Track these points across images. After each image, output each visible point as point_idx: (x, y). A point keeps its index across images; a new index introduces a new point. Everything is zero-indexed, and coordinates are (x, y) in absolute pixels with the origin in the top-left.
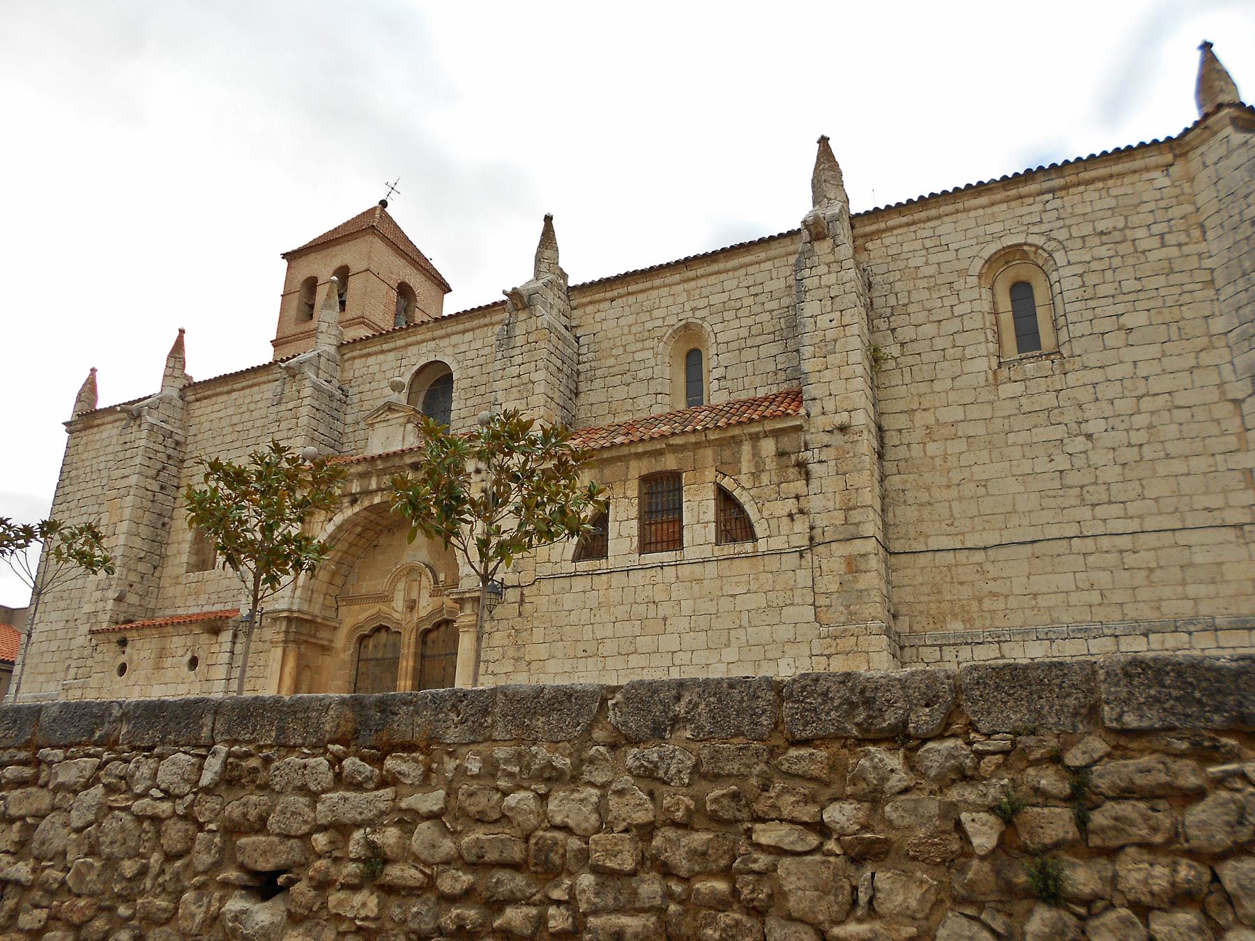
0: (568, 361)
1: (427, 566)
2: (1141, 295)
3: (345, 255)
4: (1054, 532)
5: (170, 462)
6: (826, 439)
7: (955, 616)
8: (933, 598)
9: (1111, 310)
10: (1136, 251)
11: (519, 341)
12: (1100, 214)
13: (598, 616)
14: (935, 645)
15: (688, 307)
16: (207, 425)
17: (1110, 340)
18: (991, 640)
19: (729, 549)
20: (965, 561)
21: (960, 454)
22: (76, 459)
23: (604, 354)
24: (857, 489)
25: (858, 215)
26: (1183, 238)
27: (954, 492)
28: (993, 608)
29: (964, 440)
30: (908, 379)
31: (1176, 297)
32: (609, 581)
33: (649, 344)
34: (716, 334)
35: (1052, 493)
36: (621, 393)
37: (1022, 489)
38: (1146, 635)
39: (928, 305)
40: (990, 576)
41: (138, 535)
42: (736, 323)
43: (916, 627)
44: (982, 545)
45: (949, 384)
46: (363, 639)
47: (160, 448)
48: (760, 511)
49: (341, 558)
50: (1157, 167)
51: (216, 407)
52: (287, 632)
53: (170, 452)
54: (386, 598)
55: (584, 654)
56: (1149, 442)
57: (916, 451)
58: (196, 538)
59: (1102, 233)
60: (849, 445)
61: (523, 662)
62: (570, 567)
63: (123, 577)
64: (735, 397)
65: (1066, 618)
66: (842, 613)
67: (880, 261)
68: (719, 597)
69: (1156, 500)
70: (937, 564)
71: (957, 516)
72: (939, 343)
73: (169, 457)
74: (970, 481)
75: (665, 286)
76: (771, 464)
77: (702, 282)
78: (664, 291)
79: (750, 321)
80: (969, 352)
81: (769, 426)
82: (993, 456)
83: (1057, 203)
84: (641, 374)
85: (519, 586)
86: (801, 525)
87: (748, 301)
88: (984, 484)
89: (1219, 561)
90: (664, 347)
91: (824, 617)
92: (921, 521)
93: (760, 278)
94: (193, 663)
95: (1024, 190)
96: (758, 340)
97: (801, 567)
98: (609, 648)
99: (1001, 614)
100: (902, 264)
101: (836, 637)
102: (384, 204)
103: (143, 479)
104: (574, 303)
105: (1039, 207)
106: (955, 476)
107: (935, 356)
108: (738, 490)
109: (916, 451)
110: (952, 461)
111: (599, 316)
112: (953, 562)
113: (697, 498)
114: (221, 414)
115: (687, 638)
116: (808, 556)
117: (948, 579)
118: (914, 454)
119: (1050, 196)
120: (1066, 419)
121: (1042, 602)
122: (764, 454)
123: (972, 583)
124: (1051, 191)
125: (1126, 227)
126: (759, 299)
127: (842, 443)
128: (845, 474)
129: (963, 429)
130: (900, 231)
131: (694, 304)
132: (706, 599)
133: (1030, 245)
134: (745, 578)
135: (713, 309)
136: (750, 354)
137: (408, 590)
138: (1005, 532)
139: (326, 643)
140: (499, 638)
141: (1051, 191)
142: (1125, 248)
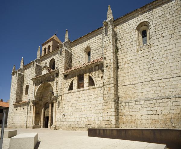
9: (160, 33)
10: (166, 19)
12: (160, 12)
17: (159, 39)
26: (177, 14)
27: (130, 74)
33: (82, 51)
35: (147, 72)
36: (78, 61)
38: (162, 99)
39: (127, 37)
40: (134, 89)
59: (160, 16)
62: (68, 92)
72: (128, 44)
79: (97, 45)
91: (105, 99)
100: (122, 29)
107: (127, 47)
115: (84, 103)
136: (97, 51)
142: (164, 19)
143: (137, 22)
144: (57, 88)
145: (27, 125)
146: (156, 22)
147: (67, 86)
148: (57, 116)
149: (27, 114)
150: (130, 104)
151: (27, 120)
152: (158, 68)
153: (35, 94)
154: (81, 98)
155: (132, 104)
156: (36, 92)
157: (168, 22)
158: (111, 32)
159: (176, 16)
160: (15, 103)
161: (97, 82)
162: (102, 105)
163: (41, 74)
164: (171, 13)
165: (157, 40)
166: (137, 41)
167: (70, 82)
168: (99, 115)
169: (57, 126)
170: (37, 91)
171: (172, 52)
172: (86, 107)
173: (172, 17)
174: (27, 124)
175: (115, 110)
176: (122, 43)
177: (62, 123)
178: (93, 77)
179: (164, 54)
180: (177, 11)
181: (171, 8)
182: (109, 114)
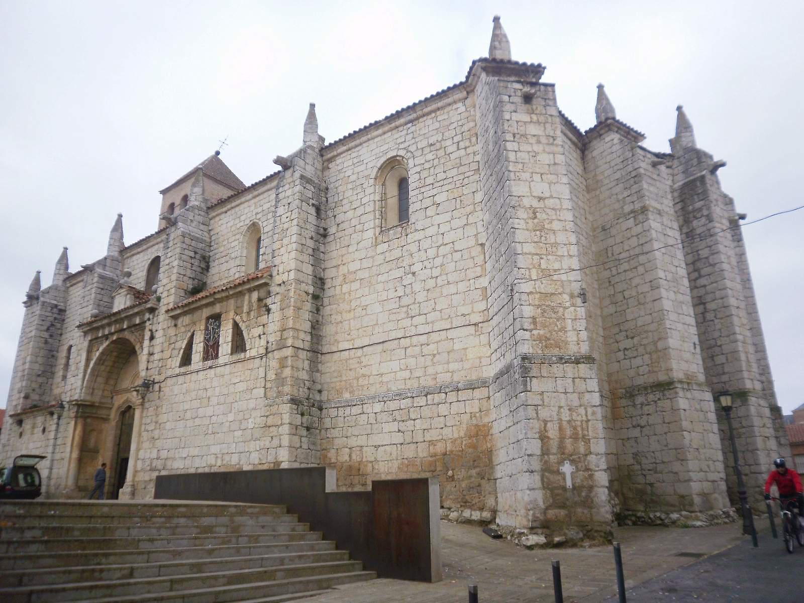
0: (200, 252)
2: (446, 182)
3: (186, 189)
4: (393, 335)
5: (56, 321)
9: (431, 193)
10: (446, 154)
12: (431, 133)
14: (335, 407)
17: (430, 212)
26: (467, 144)
30: (338, 247)
31: (461, 181)
33: (237, 237)
35: (394, 311)
38: (426, 396)
39: (351, 199)
40: (363, 364)
41: (36, 362)
43: (330, 397)
47: (50, 314)
50: (460, 100)
52: (77, 412)
56: (441, 275)
59: (431, 145)
62: (177, 371)
65: (394, 388)
69: (441, 311)
71: (352, 329)
72: (354, 222)
73: (55, 319)
76: (255, 306)
77: (261, 197)
83: (413, 129)
86: (263, 342)
88: (365, 308)
89: (465, 347)
90: (243, 238)
95: (398, 123)
102: (218, 153)
104: (210, 216)
105: (405, 132)
106: (353, 304)
107: (351, 230)
113: (226, 329)
116: (264, 359)
119: (410, 125)
124: (411, 121)
125: (443, 140)
129: (360, 275)
130: (344, 155)
131: (257, 211)
133: (400, 156)
138: (372, 337)
139: (105, 417)
141: (411, 121)
142: (441, 153)
144: (152, 358)
146: (423, 161)
148: (141, 454)
152: (421, 297)
154: (209, 393)
157: (449, 165)
159: (465, 148)
161: (253, 342)
163: (111, 305)
164: (456, 139)
165: (422, 213)
166: (377, 212)
167: (187, 338)
168: (253, 446)
170: (93, 369)
171: (456, 251)
173: (458, 149)
176: (339, 220)
178: (243, 326)
179: (438, 256)
180: (469, 137)
181: (455, 125)
182: (276, 442)
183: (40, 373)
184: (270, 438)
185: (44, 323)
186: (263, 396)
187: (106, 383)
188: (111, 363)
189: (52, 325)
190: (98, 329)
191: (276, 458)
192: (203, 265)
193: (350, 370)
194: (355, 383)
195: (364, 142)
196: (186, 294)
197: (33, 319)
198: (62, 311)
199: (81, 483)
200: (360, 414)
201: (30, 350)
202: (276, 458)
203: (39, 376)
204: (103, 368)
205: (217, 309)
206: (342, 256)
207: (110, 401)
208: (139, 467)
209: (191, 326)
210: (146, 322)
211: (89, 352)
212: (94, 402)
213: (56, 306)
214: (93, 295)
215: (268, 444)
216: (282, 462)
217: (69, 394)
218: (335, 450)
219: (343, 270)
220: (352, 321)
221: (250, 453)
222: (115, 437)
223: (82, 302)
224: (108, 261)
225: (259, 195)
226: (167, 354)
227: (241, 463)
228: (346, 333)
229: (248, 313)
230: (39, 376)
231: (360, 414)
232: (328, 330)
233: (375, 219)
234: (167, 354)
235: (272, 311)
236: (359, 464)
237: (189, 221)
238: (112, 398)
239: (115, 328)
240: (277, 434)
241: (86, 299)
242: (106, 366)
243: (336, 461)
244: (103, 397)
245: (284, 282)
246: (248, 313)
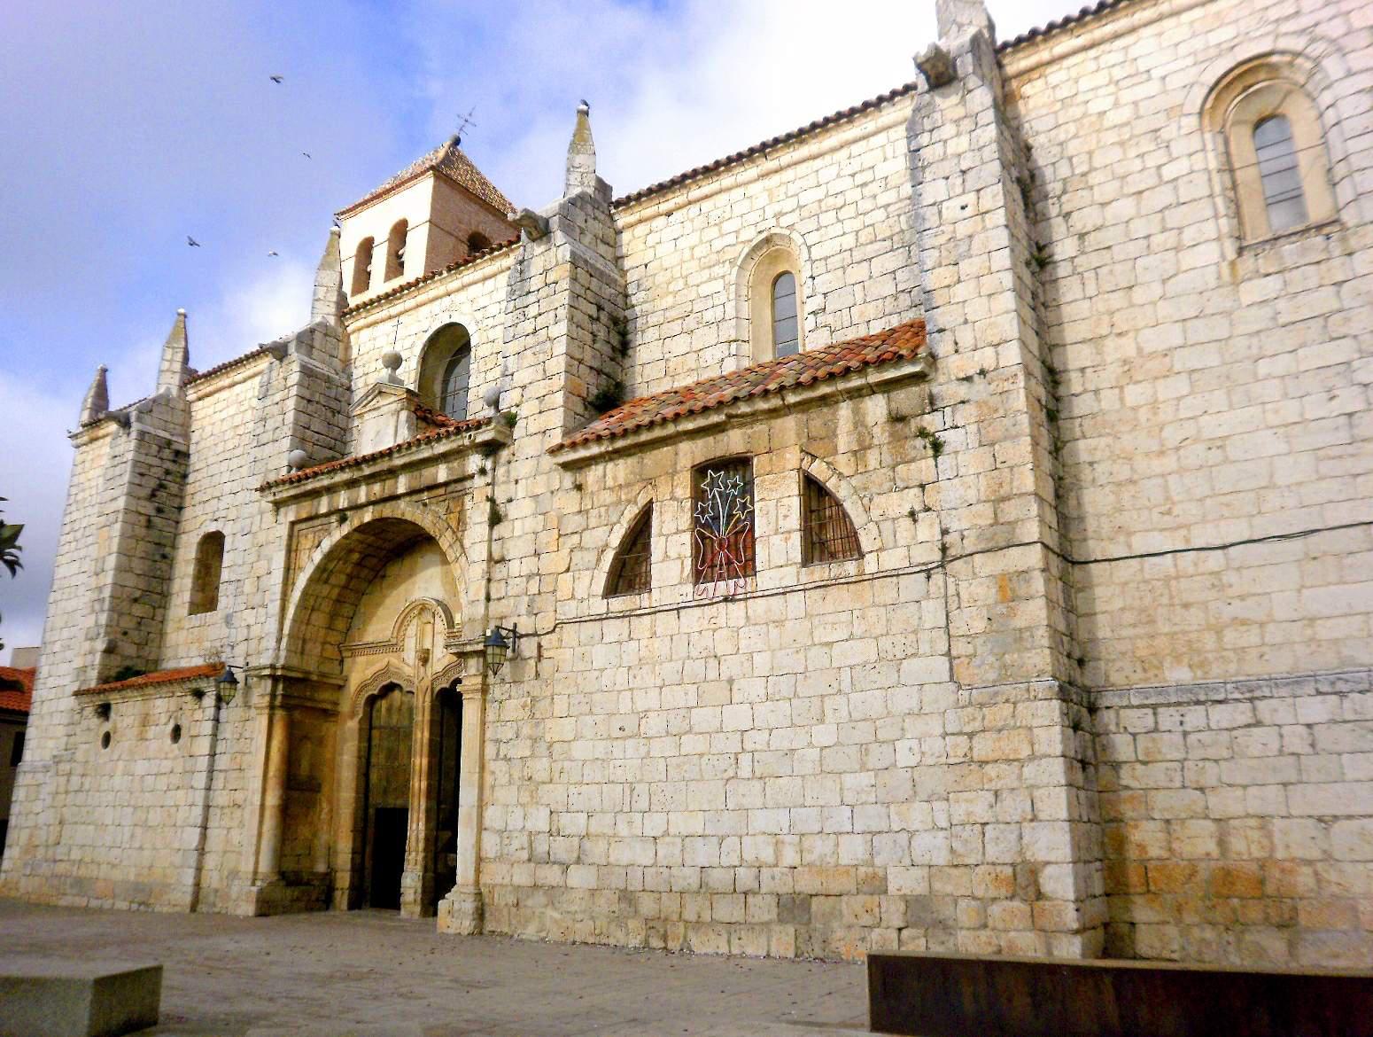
0: (608, 306)
1: (437, 601)
5: (169, 478)
6: (963, 391)
7: (1178, 659)
8: (1140, 631)
11: (535, 283)
13: (638, 678)
15: (770, 212)
16: (208, 430)
18: (1237, 695)
19: (820, 572)
20: (1191, 570)
21: (1179, 399)
22: (82, 478)
23: (659, 291)
24: (1011, 468)
25: (1005, 45)
27: (1169, 462)
28: (1242, 643)
29: (1184, 376)
30: (1091, 290)
32: (653, 625)
33: (718, 270)
34: (809, 248)
36: (679, 346)
37: (1283, 448)
39: (1120, 171)
41: (130, 570)
42: (838, 229)
44: (1219, 543)
45: (1157, 290)
46: (372, 701)
47: (156, 461)
48: (867, 510)
49: (339, 595)
51: (219, 406)
53: (169, 465)
54: (393, 646)
55: (620, 734)
57: (1109, 400)
58: (199, 571)
60: (997, 398)
61: (542, 743)
62: (599, 606)
63: (114, 623)
64: (841, 337)
66: (991, 666)
67: (1044, 111)
68: (807, 648)
70: (1147, 576)
71: (1176, 498)
72: (1139, 229)
73: (167, 472)
74: (1196, 440)
75: (738, 186)
76: (881, 435)
77: (788, 175)
78: (737, 194)
79: (857, 224)
80: (1189, 236)
81: (874, 377)
82: (1235, 399)
84: (709, 316)
85: (535, 634)
86: (927, 530)
87: (854, 195)
88: (1219, 443)
91: (964, 675)
92: (1120, 510)
93: (868, 160)
94: (177, 733)
96: (870, 250)
97: (928, 595)
98: (654, 724)
99: (1254, 653)
100: (1076, 112)
101: (982, 706)
103: (134, 502)
106: (1172, 435)
107: (1133, 249)
108: (834, 480)
109: (1109, 400)
110: (1166, 413)
111: (652, 239)
112: (1172, 571)
113: (775, 495)
114: (223, 415)
115: (763, 710)
116: (938, 578)
117: (1165, 600)
118: (1104, 405)
120: (1354, 328)
121: (1324, 631)
122: (870, 420)
123: (1204, 605)
126: (867, 191)
127: (984, 396)
128: (992, 444)
129: (1182, 360)
131: (776, 208)
132: (790, 651)
133: (1283, 53)
134: (844, 617)
135: (805, 213)
136: (859, 273)
137: (421, 637)
138: (1257, 521)
139: (329, 707)
140: (513, 709)
143: (1201, 57)
144: (499, 572)
145: (204, 884)
147: (591, 557)
149: (210, 779)
150: (1195, 717)
151: (204, 837)
153: (283, 609)
155: (1220, 715)
156: (296, 596)
158: (992, 131)
160: (93, 684)
162: (939, 730)
168: (917, 815)
169: (502, 899)
170: (305, 593)
172: (781, 741)
174: (199, 869)
175: (1069, 769)
176: (1080, 221)
177: (551, 875)
183: (138, 594)
184: (990, 797)
185: (144, 481)
186: (946, 677)
187: (330, 628)
188: (342, 579)
189: (161, 486)
190: (315, 494)
191: (1021, 852)
192: (615, 340)
193: (1186, 606)
194: (1209, 641)
195: (1145, 25)
196: (586, 408)
197: (118, 471)
198: (182, 456)
199: (290, 865)
200: (1248, 726)
201: (116, 541)
202: (1021, 852)
203: (136, 600)
204: (325, 590)
205: (734, 442)
206: (1112, 313)
207: (337, 670)
208: (490, 844)
209: (637, 488)
210: (472, 477)
211: (291, 551)
212: (309, 673)
213: (169, 443)
214: (290, 417)
215: (981, 811)
216: (1048, 863)
217: (241, 649)
218: (1159, 825)
219: (1114, 349)
220: (1172, 480)
221: (912, 834)
222: (359, 757)
223: (261, 430)
224: (318, 336)
225: (375, 323)
226: (554, 562)
227: (878, 861)
228: (1156, 511)
229: (859, 452)
230: (136, 600)
231: (1248, 726)
232: (1095, 501)
233: (1216, 217)
234: (554, 562)
235: (946, 449)
236: (1262, 867)
237: (578, 230)
238: (342, 662)
239: (367, 495)
240: (1015, 784)
241: (271, 424)
242: (334, 586)
243: (1165, 854)
244: (323, 659)
245: (982, 373)
246: (859, 452)
